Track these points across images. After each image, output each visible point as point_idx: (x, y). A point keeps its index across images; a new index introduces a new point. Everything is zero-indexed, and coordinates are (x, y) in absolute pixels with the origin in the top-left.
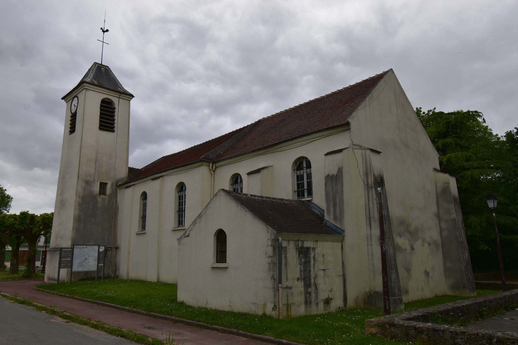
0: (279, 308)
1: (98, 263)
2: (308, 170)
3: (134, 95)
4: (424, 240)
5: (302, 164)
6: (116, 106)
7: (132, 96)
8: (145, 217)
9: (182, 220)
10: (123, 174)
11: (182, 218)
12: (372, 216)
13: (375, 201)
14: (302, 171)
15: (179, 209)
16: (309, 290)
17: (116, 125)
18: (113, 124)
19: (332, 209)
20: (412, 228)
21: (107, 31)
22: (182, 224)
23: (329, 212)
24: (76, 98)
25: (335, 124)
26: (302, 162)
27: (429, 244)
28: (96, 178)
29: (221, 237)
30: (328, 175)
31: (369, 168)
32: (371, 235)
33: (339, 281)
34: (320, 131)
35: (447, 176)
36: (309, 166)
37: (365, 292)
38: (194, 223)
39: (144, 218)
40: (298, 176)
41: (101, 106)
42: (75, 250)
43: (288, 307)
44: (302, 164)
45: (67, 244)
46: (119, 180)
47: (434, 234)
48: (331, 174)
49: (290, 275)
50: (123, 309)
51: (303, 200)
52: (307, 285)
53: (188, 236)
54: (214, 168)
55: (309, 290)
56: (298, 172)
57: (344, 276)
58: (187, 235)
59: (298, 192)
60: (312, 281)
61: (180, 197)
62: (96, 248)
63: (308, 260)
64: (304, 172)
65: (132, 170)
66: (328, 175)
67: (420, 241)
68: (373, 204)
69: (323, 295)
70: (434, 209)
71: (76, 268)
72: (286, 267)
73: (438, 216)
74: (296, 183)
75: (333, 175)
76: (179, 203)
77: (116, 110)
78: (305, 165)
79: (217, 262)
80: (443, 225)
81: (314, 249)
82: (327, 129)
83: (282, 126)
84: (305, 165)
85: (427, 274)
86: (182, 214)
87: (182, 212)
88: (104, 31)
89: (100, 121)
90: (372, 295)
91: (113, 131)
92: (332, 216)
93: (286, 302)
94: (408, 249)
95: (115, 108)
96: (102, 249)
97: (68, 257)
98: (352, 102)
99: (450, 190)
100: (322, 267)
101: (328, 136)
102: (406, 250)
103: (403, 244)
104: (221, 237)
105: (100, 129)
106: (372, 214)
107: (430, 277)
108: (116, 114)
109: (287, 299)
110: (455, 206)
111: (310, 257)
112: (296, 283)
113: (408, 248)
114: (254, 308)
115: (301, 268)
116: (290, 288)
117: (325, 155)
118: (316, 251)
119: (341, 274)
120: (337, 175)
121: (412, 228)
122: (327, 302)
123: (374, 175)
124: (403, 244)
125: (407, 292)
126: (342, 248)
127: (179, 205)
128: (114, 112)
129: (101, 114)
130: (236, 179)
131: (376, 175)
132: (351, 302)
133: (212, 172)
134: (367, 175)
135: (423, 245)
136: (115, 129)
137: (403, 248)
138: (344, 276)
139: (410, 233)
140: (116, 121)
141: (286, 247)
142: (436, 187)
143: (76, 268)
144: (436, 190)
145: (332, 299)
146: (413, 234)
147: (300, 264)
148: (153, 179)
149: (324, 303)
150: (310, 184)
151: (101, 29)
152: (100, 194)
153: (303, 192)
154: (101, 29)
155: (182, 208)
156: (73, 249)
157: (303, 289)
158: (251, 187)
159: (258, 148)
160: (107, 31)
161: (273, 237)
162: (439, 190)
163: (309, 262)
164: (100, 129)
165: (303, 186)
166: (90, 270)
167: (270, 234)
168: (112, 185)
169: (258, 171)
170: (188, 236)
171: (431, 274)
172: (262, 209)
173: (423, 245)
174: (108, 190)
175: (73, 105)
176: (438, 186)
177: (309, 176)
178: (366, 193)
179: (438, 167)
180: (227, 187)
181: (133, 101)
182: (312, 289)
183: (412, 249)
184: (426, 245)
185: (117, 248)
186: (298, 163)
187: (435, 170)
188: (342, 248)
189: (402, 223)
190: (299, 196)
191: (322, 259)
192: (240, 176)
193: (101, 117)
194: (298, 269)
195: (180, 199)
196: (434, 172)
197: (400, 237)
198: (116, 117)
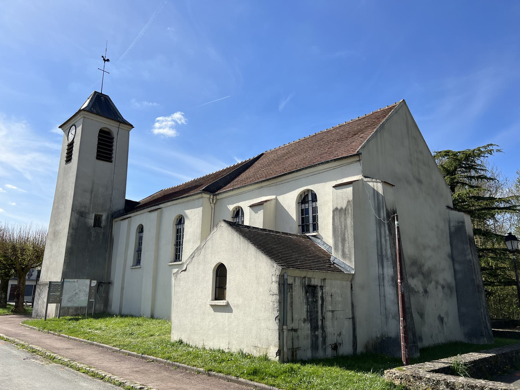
0: (283, 352)
1: (89, 299)
2: (314, 204)
3: (134, 126)
4: (437, 283)
5: (307, 199)
6: (115, 136)
7: (132, 127)
8: (141, 250)
9: (179, 255)
10: (121, 206)
11: (179, 252)
12: (384, 253)
13: (388, 238)
14: (307, 205)
15: (177, 242)
16: (317, 333)
17: (114, 155)
18: (111, 154)
19: (340, 246)
20: (425, 268)
21: (108, 60)
22: (179, 259)
23: (336, 248)
24: (74, 127)
25: (344, 155)
26: (308, 195)
27: (443, 287)
28: (91, 209)
29: (221, 273)
30: (337, 209)
31: (381, 202)
32: (383, 274)
33: (348, 324)
34: (328, 162)
35: (462, 213)
36: (315, 198)
37: (377, 337)
38: (192, 256)
39: (139, 251)
40: (302, 210)
41: (99, 135)
42: (65, 284)
43: (293, 352)
44: (307, 199)
45: (57, 278)
46: (115, 212)
47: (446, 276)
48: (339, 207)
49: (296, 316)
50: (93, 344)
51: (307, 234)
52: (314, 328)
53: (185, 270)
54: (215, 201)
55: (317, 333)
56: (303, 206)
57: (353, 318)
58: (184, 269)
59: (303, 227)
60: (320, 323)
61: (178, 230)
62: (88, 281)
63: (315, 300)
64: (310, 206)
65: (128, 202)
66: (337, 209)
67: (433, 283)
68: (386, 241)
69: (331, 340)
70: (447, 249)
71: (65, 303)
72: (292, 306)
73: (452, 257)
74: (301, 217)
75: (342, 209)
76: (177, 236)
77: (115, 140)
78: (310, 199)
79: (216, 299)
80: (457, 267)
81: (322, 287)
82: (335, 160)
83: (286, 159)
84: (310, 199)
85: (441, 319)
86: (180, 248)
87: (180, 246)
88: (105, 60)
89: (98, 151)
90: (384, 340)
91: (111, 162)
92: (340, 252)
93: (291, 347)
94: (421, 292)
95: (113, 138)
96: (94, 283)
97: (58, 291)
98: (361, 133)
99: (465, 230)
100: (330, 308)
101: (334, 168)
102: (418, 292)
103: (415, 285)
104: (221, 273)
105: (97, 158)
106: (384, 252)
107: (444, 323)
108: (115, 144)
109: (292, 343)
110: (470, 246)
111: (317, 296)
112: (303, 325)
113: (421, 290)
114: (255, 351)
115: (307, 308)
116: (295, 330)
117: (334, 187)
118: (324, 290)
119: (124, 312)
120: (346, 209)
121: (425, 268)
122: (335, 347)
123: (387, 210)
124: (415, 285)
125: (421, 339)
126: (352, 288)
127: (177, 239)
128: (112, 142)
129: (99, 143)
130: (238, 213)
131: (389, 209)
132: (360, 349)
133: (212, 205)
134: (378, 210)
135: (436, 288)
136: (113, 159)
137: (417, 290)
138: (353, 318)
139: (423, 274)
140: (114, 152)
141: (292, 284)
142: (449, 226)
143: (65, 303)
144: (450, 229)
145: (340, 344)
146: (426, 276)
147: (308, 303)
148: (150, 212)
149: (332, 349)
150: (315, 218)
151: (103, 57)
152: (94, 226)
153: (308, 226)
154: (103, 57)
155: (180, 242)
156: (63, 283)
157: (309, 332)
158: (253, 219)
159: (260, 180)
160: (108, 60)
161: (278, 273)
162: (453, 229)
163: (316, 301)
164: (97, 158)
165: (308, 220)
166: (80, 306)
167: (274, 269)
168: (108, 217)
169: (261, 204)
170: (185, 270)
171: (445, 320)
172: (265, 241)
173: (436, 288)
174: (103, 223)
175: (70, 134)
176: (452, 225)
177: (315, 210)
178: (378, 230)
179: (451, 206)
180: (230, 219)
181: (132, 132)
182: (319, 333)
183: (426, 291)
184: (440, 287)
185: (109, 283)
186: (303, 196)
187: (448, 207)
188: (352, 288)
189: (414, 263)
190: (303, 231)
191: (330, 299)
192: (242, 209)
193: (98, 147)
194: (305, 310)
195: (177, 233)
196: (448, 210)
197: (413, 278)
198: (114, 148)
